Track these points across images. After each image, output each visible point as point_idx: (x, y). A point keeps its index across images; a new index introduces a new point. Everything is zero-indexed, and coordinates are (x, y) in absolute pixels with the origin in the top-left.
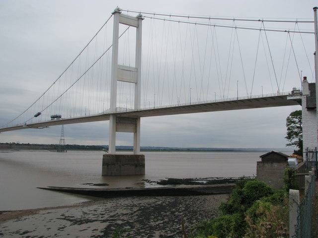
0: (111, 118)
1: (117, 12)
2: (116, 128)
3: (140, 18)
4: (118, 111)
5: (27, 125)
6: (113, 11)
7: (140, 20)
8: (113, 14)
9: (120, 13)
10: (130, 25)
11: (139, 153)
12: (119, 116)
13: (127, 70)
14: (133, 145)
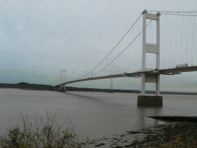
0: (143, 75)
2: (146, 80)
3: (158, 14)
4: (147, 70)
5: (126, 74)
6: (142, 12)
7: (158, 16)
8: (142, 13)
9: (146, 13)
10: (152, 19)
11: (159, 95)
12: (147, 73)
14: (155, 90)
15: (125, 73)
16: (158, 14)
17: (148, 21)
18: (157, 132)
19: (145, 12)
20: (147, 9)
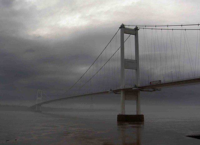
0: (122, 93)
1: (122, 27)
5: (113, 91)
8: (120, 28)
13: (130, 61)
15: (111, 90)
16: (137, 29)
17: (126, 35)
18: (186, 35)
19: (122, 27)
20: (124, 24)
